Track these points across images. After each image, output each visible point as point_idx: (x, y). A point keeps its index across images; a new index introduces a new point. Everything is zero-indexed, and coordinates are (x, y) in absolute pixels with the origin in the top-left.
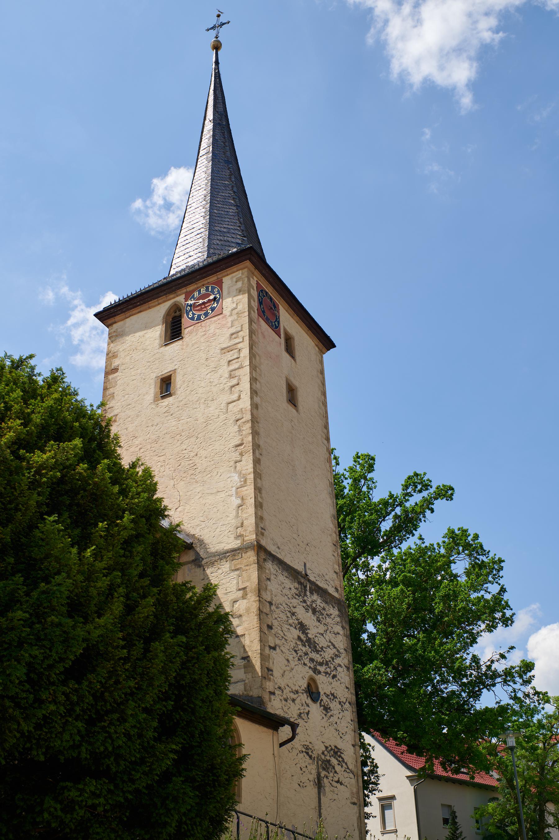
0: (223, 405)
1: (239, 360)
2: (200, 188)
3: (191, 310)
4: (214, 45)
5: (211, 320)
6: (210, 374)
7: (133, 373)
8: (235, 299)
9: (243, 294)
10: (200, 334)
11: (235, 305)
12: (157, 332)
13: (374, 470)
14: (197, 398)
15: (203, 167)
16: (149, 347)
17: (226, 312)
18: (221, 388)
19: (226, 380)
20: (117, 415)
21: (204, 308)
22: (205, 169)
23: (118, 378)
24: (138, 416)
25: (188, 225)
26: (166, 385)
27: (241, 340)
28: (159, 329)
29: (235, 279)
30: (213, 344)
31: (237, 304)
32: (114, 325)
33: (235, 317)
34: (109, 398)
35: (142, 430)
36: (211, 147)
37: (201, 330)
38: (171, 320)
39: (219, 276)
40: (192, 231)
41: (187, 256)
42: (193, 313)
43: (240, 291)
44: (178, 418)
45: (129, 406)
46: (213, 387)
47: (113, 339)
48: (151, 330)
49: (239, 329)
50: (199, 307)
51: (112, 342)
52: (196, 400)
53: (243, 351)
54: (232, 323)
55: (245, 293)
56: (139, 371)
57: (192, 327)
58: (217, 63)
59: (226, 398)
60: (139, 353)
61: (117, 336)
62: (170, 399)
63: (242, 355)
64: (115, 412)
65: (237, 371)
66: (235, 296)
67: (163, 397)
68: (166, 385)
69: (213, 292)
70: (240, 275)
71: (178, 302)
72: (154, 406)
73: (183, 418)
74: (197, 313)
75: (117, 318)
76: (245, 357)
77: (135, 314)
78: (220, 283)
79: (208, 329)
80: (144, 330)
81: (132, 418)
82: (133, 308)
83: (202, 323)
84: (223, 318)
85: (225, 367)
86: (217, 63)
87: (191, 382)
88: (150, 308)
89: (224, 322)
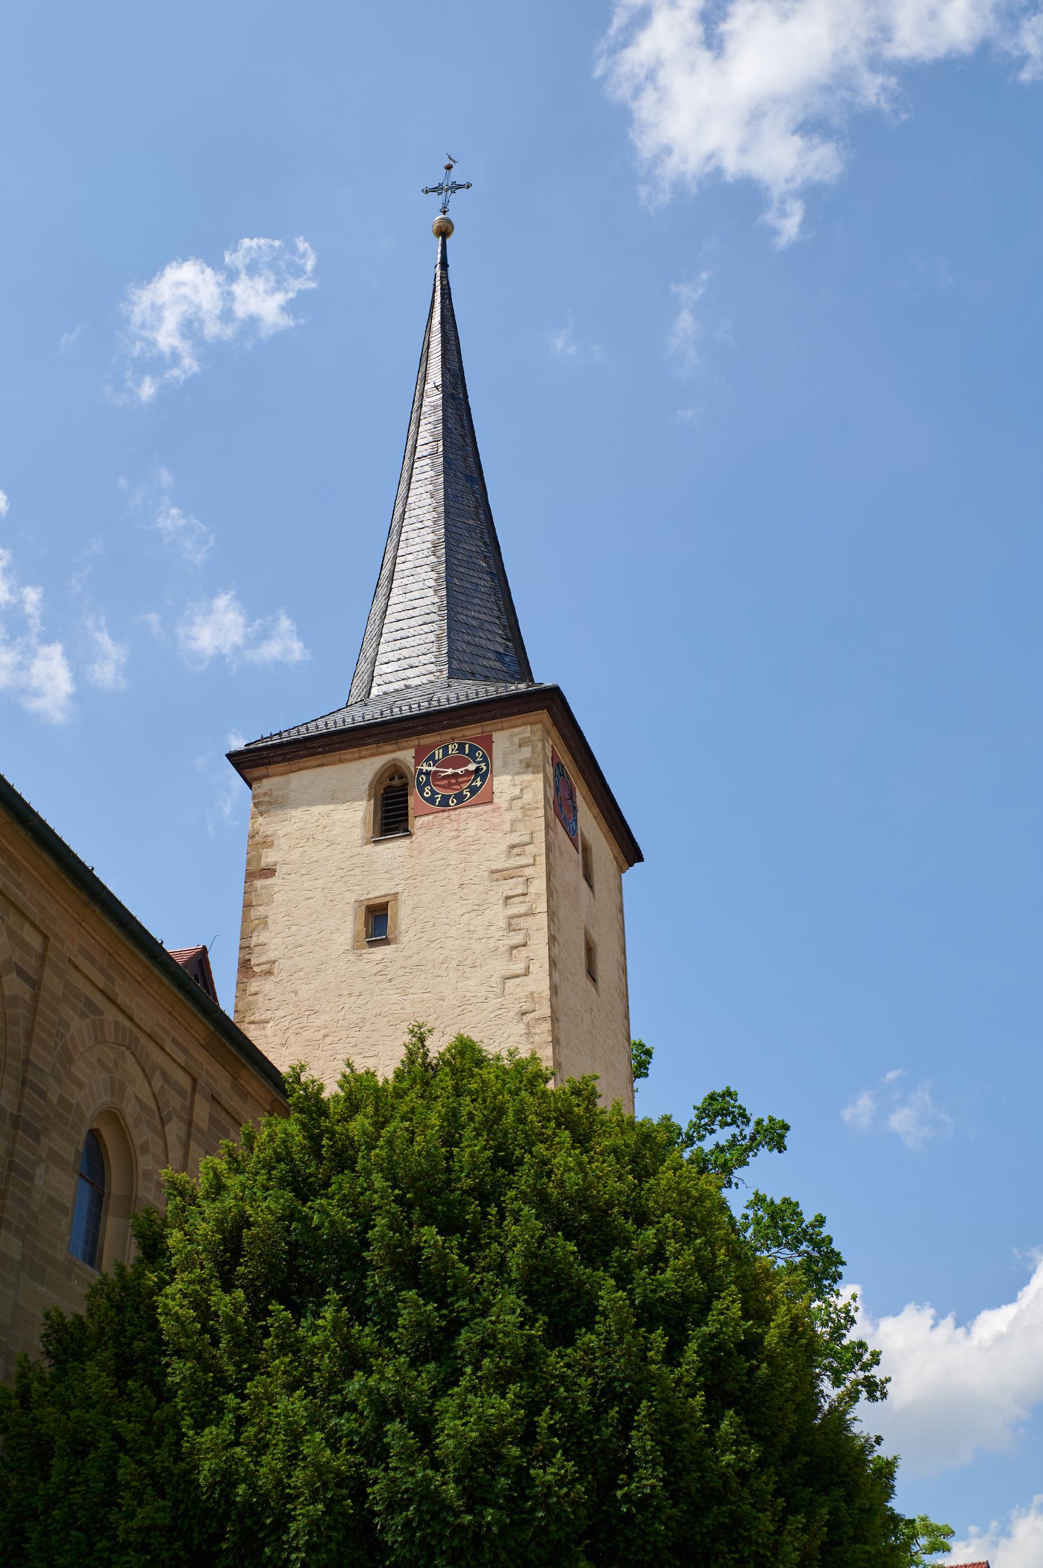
0: (495, 980)
1: (527, 898)
2: (420, 525)
3: (427, 783)
4: (440, 227)
5: (469, 809)
6: (467, 916)
7: (306, 885)
8: (519, 779)
9: (533, 773)
10: (448, 832)
11: (517, 791)
12: (357, 814)
13: (647, 1075)
14: (443, 957)
15: (427, 482)
16: (340, 839)
17: (501, 800)
18: (490, 946)
19: (502, 933)
20: (274, 962)
21: (454, 784)
22: (431, 487)
23: (276, 889)
24: (318, 971)
25: (401, 599)
26: (377, 922)
27: (531, 861)
28: (362, 808)
29: (516, 740)
30: (475, 858)
31: (522, 790)
32: (265, 781)
33: (517, 814)
34: (257, 926)
35: (329, 1001)
36: (441, 443)
37: (448, 826)
38: (382, 791)
39: (486, 729)
40: (411, 613)
41: (404, 664)
42: (431, 790)
43: (528, 766)
44: (404, 989)
45: (300, 949)
46: (474, 941)
47: (263, 808)
48: (345, 806)
49: (526, 839)
50: (446, 782)
51: (261, 814)
52: (440, 959)
53: (535, 882)
54: (512, 825)
55: (538, 772)
56: (320, 883)
57: (431, 817)
58: (444, 264)
59: (500, 967)
60: (320, 847)
61: (270, 803)
62: (387, 949)
63: (532, 890)
64: (272, 956)
65: (522, 920)
66: (518, 774)
67: (372, 944)
68: (377, 922)
69: (472, 754)
70: (528, 734)
71: (400, 761)
72: (352, 958)
73: (413, 990)
74: (441, 792)
75: (273, 769)
76: (538, 895)
77: (309, 768)
78: (487, 742)
79: (462, 826)
80: (330, 803)
81: (306, 974)
82: (309, 756)
83: (451, 812)
84: (494, 810)
85: (499, 907)
86: (444, 264)
87: (430, 924)
88: (341, 761)
89: (496, 820)
